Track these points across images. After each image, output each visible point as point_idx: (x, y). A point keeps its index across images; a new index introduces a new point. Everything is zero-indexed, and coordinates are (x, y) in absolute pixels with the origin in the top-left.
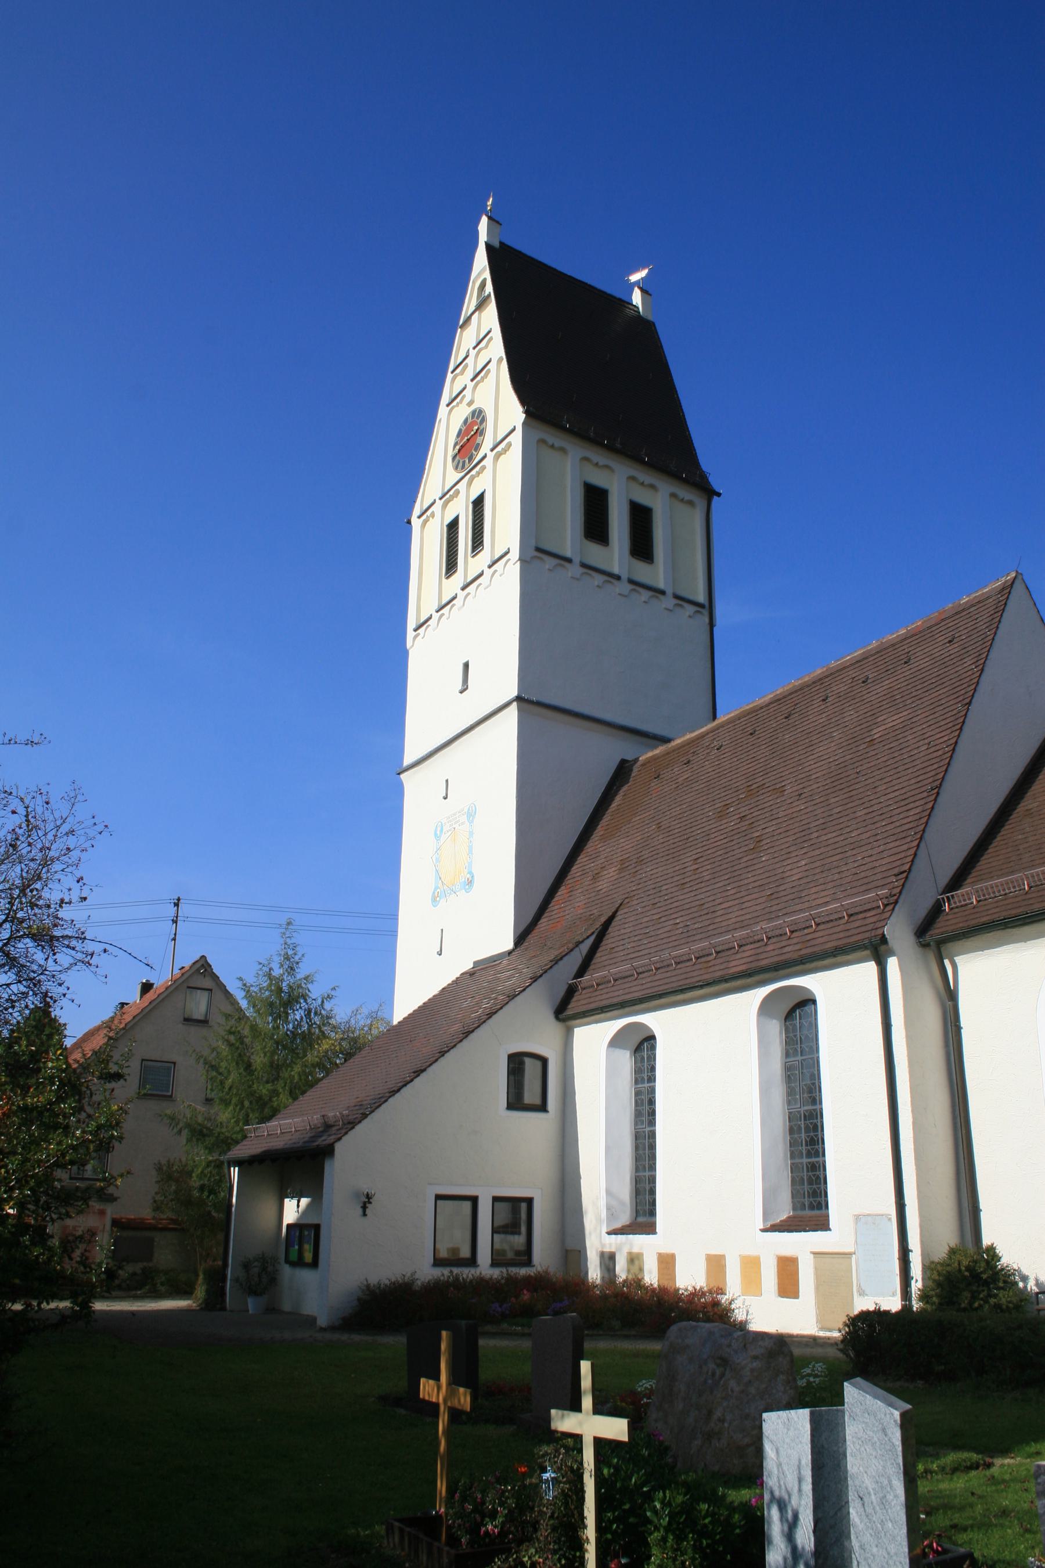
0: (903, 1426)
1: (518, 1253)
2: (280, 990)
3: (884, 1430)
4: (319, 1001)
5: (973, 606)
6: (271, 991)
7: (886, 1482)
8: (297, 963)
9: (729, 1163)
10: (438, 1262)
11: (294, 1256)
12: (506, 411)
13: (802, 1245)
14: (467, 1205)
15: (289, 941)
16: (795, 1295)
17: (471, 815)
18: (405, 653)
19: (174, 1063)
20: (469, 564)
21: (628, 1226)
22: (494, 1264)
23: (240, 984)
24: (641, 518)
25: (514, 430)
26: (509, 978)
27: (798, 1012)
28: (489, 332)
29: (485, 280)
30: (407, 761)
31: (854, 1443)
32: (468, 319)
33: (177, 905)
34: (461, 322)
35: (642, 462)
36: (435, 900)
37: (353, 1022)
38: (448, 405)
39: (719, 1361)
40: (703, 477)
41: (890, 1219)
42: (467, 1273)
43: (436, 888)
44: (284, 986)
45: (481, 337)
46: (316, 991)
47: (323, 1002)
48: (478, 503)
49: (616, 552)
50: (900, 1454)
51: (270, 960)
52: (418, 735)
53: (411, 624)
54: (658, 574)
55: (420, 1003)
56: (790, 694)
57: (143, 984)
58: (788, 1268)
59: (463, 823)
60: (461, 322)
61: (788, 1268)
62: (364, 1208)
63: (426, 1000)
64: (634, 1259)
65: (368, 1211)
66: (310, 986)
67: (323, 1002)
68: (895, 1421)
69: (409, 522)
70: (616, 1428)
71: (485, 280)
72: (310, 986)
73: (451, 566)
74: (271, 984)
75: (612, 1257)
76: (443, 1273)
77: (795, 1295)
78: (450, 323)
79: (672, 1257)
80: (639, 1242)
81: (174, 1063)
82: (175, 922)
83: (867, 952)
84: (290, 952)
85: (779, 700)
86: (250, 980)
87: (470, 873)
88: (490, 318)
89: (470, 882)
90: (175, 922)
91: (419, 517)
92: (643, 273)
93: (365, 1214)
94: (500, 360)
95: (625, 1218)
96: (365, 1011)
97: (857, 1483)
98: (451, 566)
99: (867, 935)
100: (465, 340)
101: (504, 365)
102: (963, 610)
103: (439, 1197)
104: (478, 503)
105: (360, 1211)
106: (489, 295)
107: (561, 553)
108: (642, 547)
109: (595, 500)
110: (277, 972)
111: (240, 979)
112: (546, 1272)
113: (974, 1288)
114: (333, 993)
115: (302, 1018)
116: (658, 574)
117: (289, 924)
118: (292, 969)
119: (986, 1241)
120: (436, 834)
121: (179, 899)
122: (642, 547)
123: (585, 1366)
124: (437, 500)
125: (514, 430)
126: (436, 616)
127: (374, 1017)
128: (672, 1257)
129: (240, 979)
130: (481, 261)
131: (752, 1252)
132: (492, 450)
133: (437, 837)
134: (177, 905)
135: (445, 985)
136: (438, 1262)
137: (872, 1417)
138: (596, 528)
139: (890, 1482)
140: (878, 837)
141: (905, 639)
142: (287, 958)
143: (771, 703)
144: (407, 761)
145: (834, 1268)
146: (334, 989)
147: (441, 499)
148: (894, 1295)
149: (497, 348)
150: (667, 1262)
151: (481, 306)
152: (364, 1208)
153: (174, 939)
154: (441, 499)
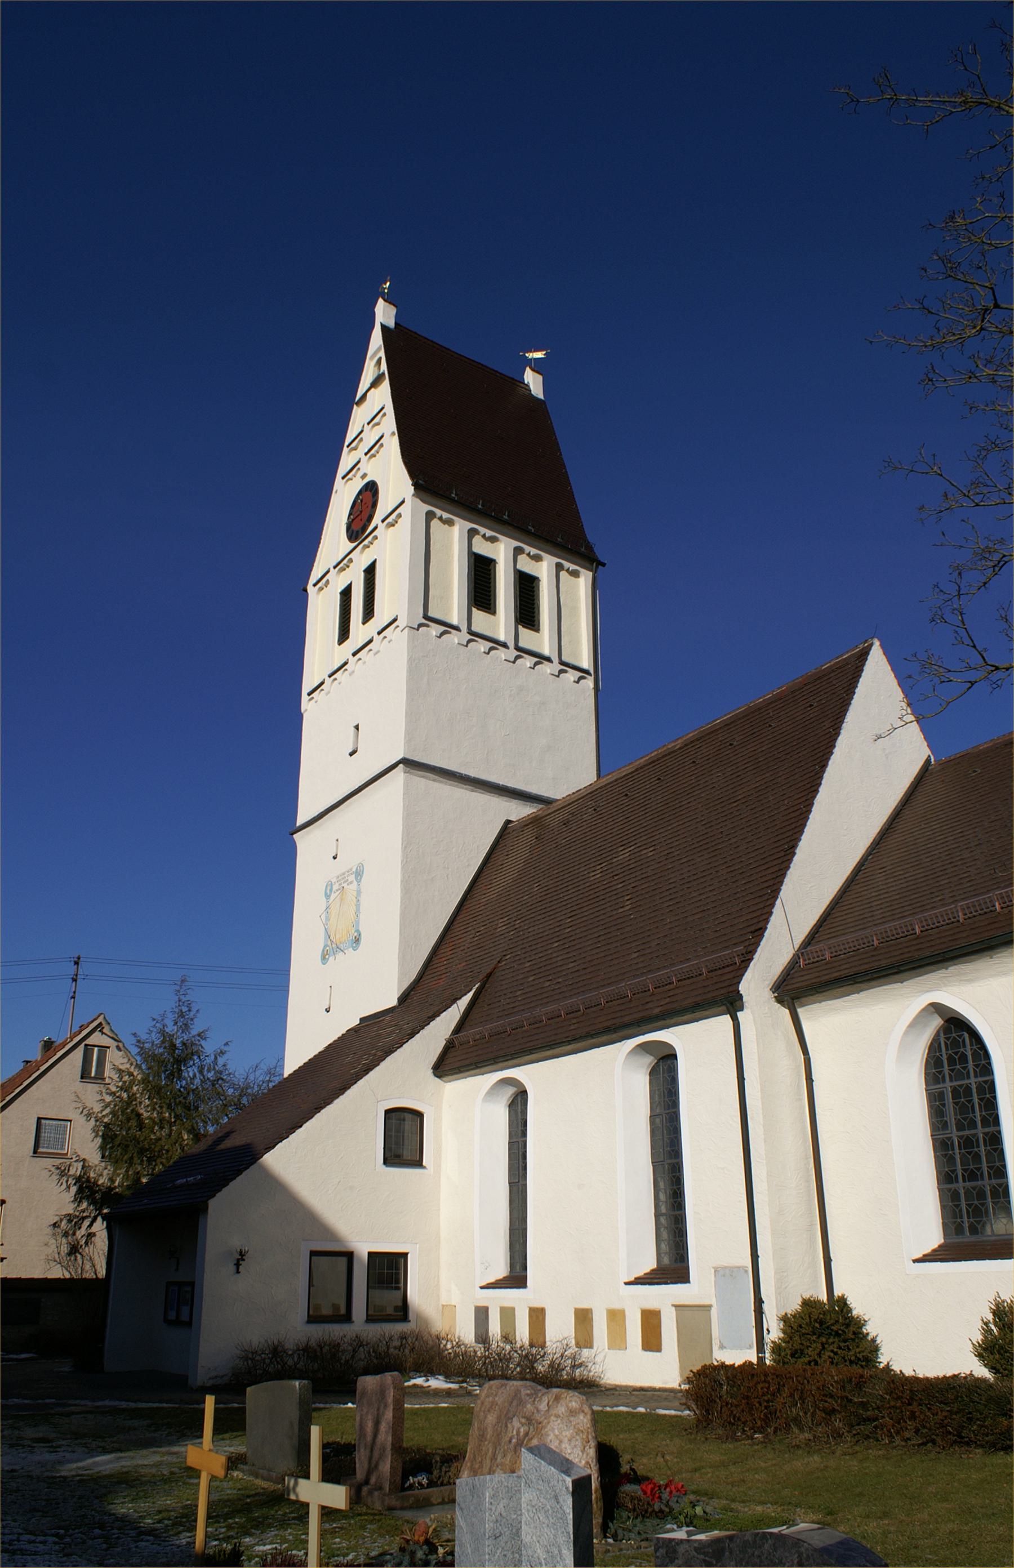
0: (574, 1494)
1: (396, 1309)
2: (173, 1046)
3: (556, 1497)
4: (213, 1057)
5: (833, 671)
6: (165, 1048)
7: (556, 1552)
8: (192, 1020)
9: (545, 1218)
10: (313, 1319)
11: (172, 1316)
12: (395, 482)
13: (664, 1297)
14: (344, 1260)
15: (184, 999)
16: (658, 1348)
17: (359, 874)
18: (300, 717)
19: (39, 1119)
20: (359, 632)
21: (505, 1279)
22: (370, 1319)
23: (134, 1040)
24: (526, 587)
25: (403, 502)
26: (392, 1032)
27: (664, 1067)
28: (383, 408)
29: (380, 359)
30: (300, 821)
31: (528, 1511)
32: (364, 396)
33: (76, 963)
34: (357, 398)
35: (528, 533)
36: (324, 958)
37: (251, 1077)
38: (343, 478)
39: (523, 1420)
40: (590, 548)
41: (746, 1271)
42: (336, 1331)
43: (326, 946)
44: (178, 1042)
45: (374, 414)
46: (209, 1047)
47: (216, 1058)
48: (370, 572)
49: (501, 622)
50: (571, 1522)
51: (163, 1016)
52: (311, 797)
53: (306, 688)
54: (543, 641)
55: (306, 1060)
56: (664, 756)
57: (45, 1041)
58: (651, 1321)
59: (351, 883)
60: (357, 398)
61: (651, 1321)
62: (238, 1265)
63: (311, 1056)
64: (508, 1314)
65: (241, 1268)
66: (203, 1042)
67: (216, 1058)
68: (567, 1488)
69: (305, 590)
70: (337, 1496)
71: (380, 359)
72: (203, 1042)
73: (344, 633)
74: (163, 1042)
75: (486, 1310)
76: (319, 1332)
77: (658, 1348)
78: (347, 399)
79: (542, 1311)
80: (510, 1296)
81: (39, 1119)
82: (75, 980)
83: (724, 1008)
84: (184, 1009)
85: (653, 762)
86: (144, 1037)
87: (358, 931)
88: (382, 397)
89: (357, 940)
90: (75, 980)
91: (315, 585)
92: (539, 355)
93: (238, 1272)
94: (393, 434)
95: (649, 1263)
96: (264, 1067)
97: (530, 1552)
98: (344, 633)
99: (723, 991)
100: (359, 416)
101: (396, 440)
102: (825, 675)
103: (313, 1253)
104: (370, 572)
105: (233, 1268)
106: (383, 374)
107: (448, 621)
108: (527, 614)
109: (481, 570)
110: (171, 1028)
111: (134, 1035)
112: (808, 1304)
113: (824, 1340)
114: (226, 1048)
115: (195, 1075)
116: (543, 641)
117: (183, 981)
118: (186, 1025)
119: (837, 1292)
120: (326, 894)
121: (79, 958)
122: (527, 614)
123: (315, 1431)
124: (332, 569)
125: (403, 502)
126: (328, 681)
127: (271, 1072)
128: (542, 1311)
129: (134, 1035)
130: (376, 340)
131: (616, 1306)
132: (383, 521)
133: (327, 896)
134: (76, 963)
135: (331, 1041)
136: (313, 1319)
137: (546, 1485)
138: (481, 594)
139: (560, 1551)
140: (738, 895)
141: (771, 703)
142: (182, 1015)
143: (645, 766)
144: (300, 821)
145: (694, 1319)
146: (227, 1044)
147: (335, 567)
148: (751, 1347)
149: (389, 423)
150: (537, 1315)
151: (375, 383)
152: (238, 1265)
153: (73, 997)
154: (335, 567)
